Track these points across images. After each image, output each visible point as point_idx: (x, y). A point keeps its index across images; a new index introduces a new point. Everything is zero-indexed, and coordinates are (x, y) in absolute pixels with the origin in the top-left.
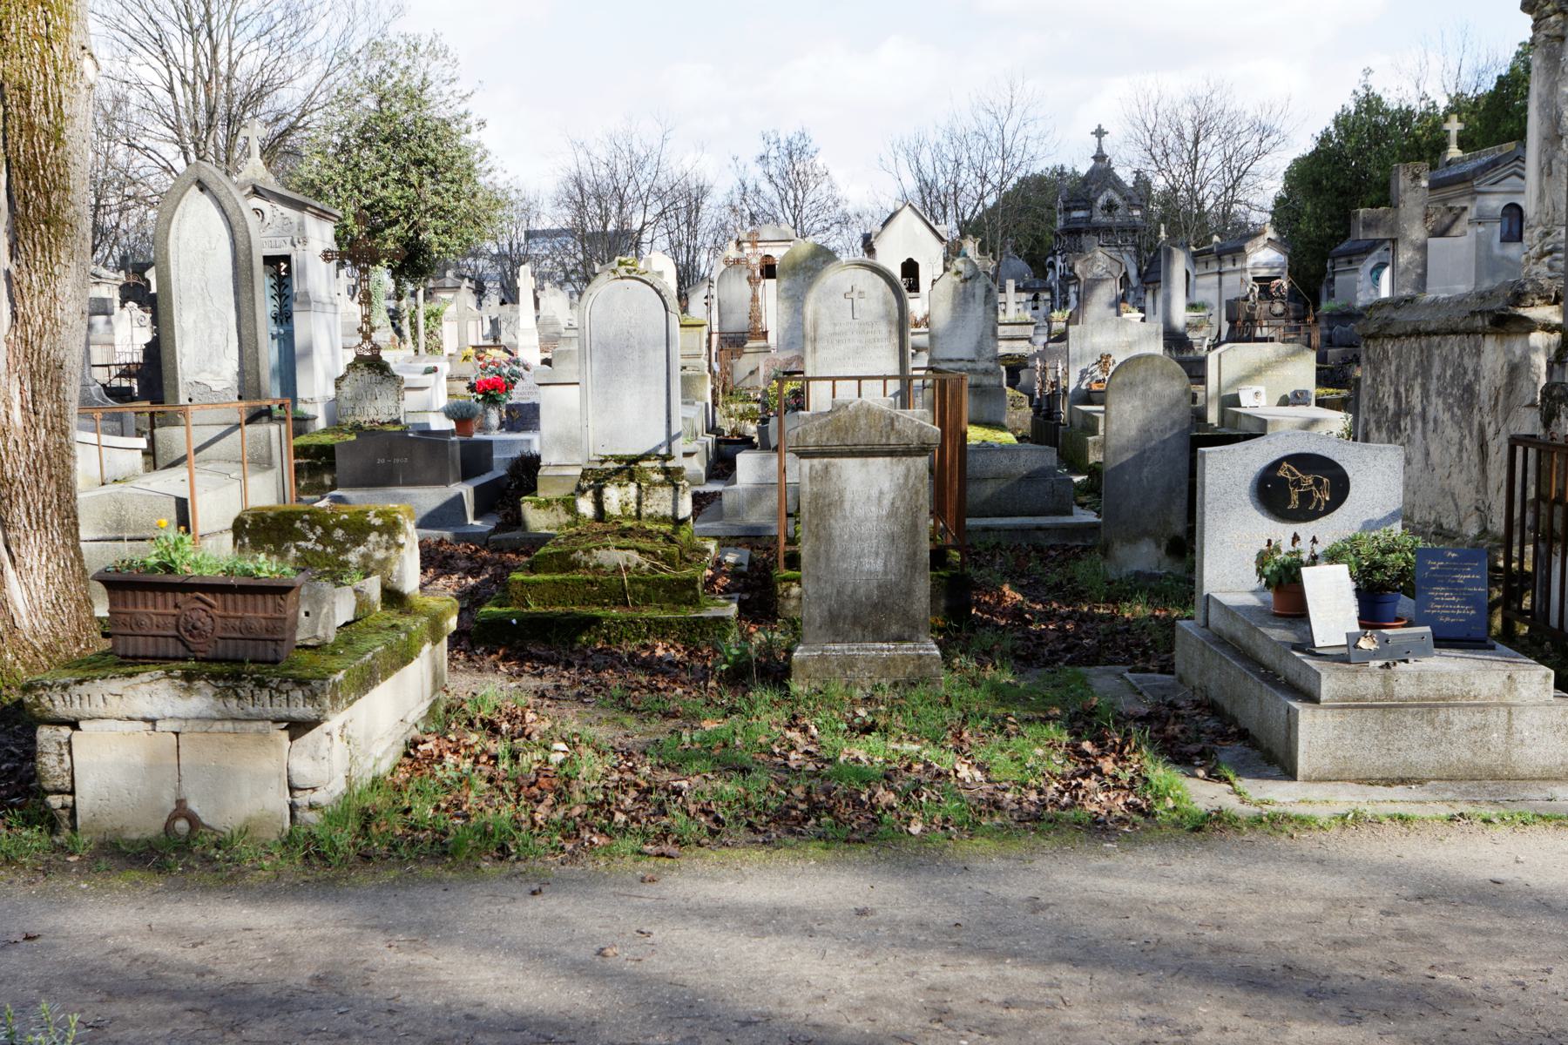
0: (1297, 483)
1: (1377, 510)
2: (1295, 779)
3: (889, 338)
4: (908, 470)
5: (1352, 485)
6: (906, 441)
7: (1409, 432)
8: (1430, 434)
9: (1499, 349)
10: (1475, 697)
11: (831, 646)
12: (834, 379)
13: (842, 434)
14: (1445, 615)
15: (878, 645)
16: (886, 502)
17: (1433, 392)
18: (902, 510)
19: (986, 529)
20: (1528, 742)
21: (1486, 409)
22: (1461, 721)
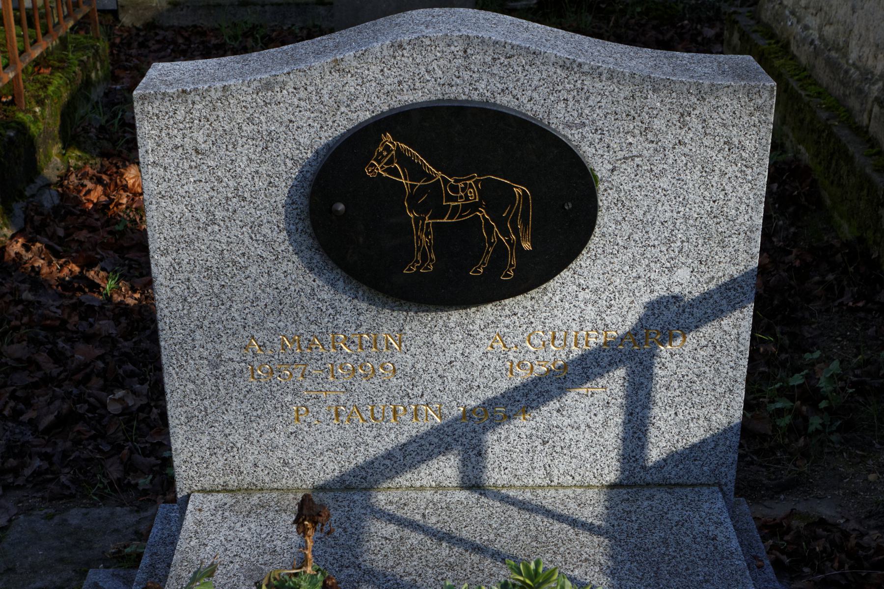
1: (683, 274)
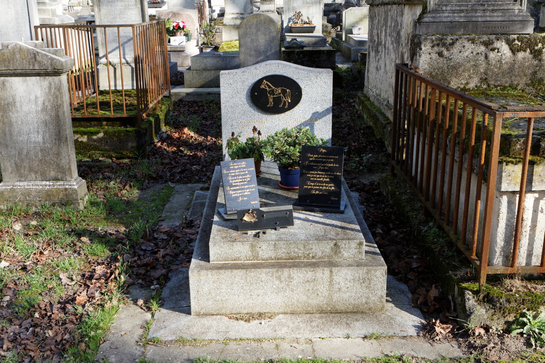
0: (272, 92)
2: (189, 313)
3: (136, 5)
4: (50, 84)
5: (303, 93)
6: (44, 67)
7: (380, 53)
8: (387, 56)
9: (410, 13)
10: (313, 257)
11: (18, 183)
12: (118, 26)
13: (7, 63)
14: (316, 190)
15: (44, 183)
16: (40, 102)
17: (388, 34)
18: (49, 107)
19: (209, 94)
20: (344, 289)
21: (404, 45)
22: (299, 277)
